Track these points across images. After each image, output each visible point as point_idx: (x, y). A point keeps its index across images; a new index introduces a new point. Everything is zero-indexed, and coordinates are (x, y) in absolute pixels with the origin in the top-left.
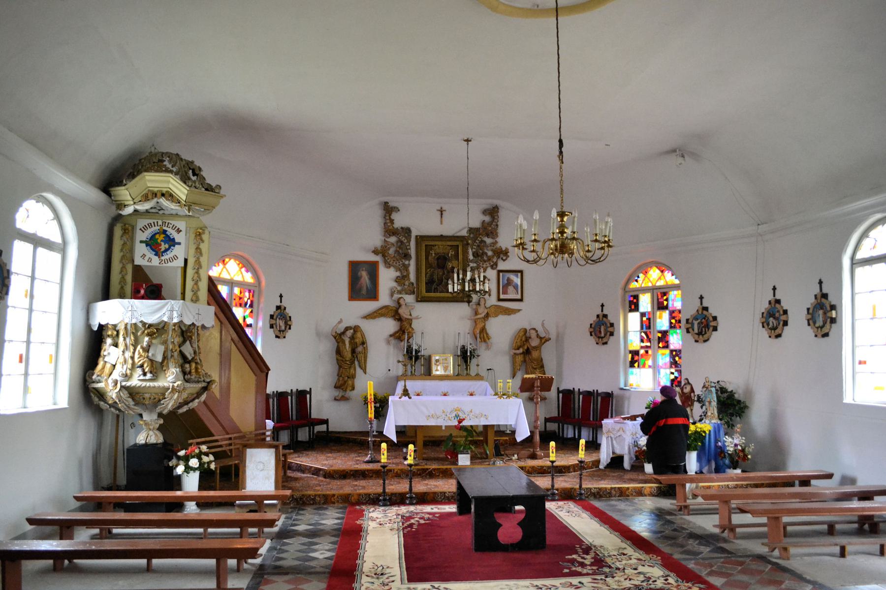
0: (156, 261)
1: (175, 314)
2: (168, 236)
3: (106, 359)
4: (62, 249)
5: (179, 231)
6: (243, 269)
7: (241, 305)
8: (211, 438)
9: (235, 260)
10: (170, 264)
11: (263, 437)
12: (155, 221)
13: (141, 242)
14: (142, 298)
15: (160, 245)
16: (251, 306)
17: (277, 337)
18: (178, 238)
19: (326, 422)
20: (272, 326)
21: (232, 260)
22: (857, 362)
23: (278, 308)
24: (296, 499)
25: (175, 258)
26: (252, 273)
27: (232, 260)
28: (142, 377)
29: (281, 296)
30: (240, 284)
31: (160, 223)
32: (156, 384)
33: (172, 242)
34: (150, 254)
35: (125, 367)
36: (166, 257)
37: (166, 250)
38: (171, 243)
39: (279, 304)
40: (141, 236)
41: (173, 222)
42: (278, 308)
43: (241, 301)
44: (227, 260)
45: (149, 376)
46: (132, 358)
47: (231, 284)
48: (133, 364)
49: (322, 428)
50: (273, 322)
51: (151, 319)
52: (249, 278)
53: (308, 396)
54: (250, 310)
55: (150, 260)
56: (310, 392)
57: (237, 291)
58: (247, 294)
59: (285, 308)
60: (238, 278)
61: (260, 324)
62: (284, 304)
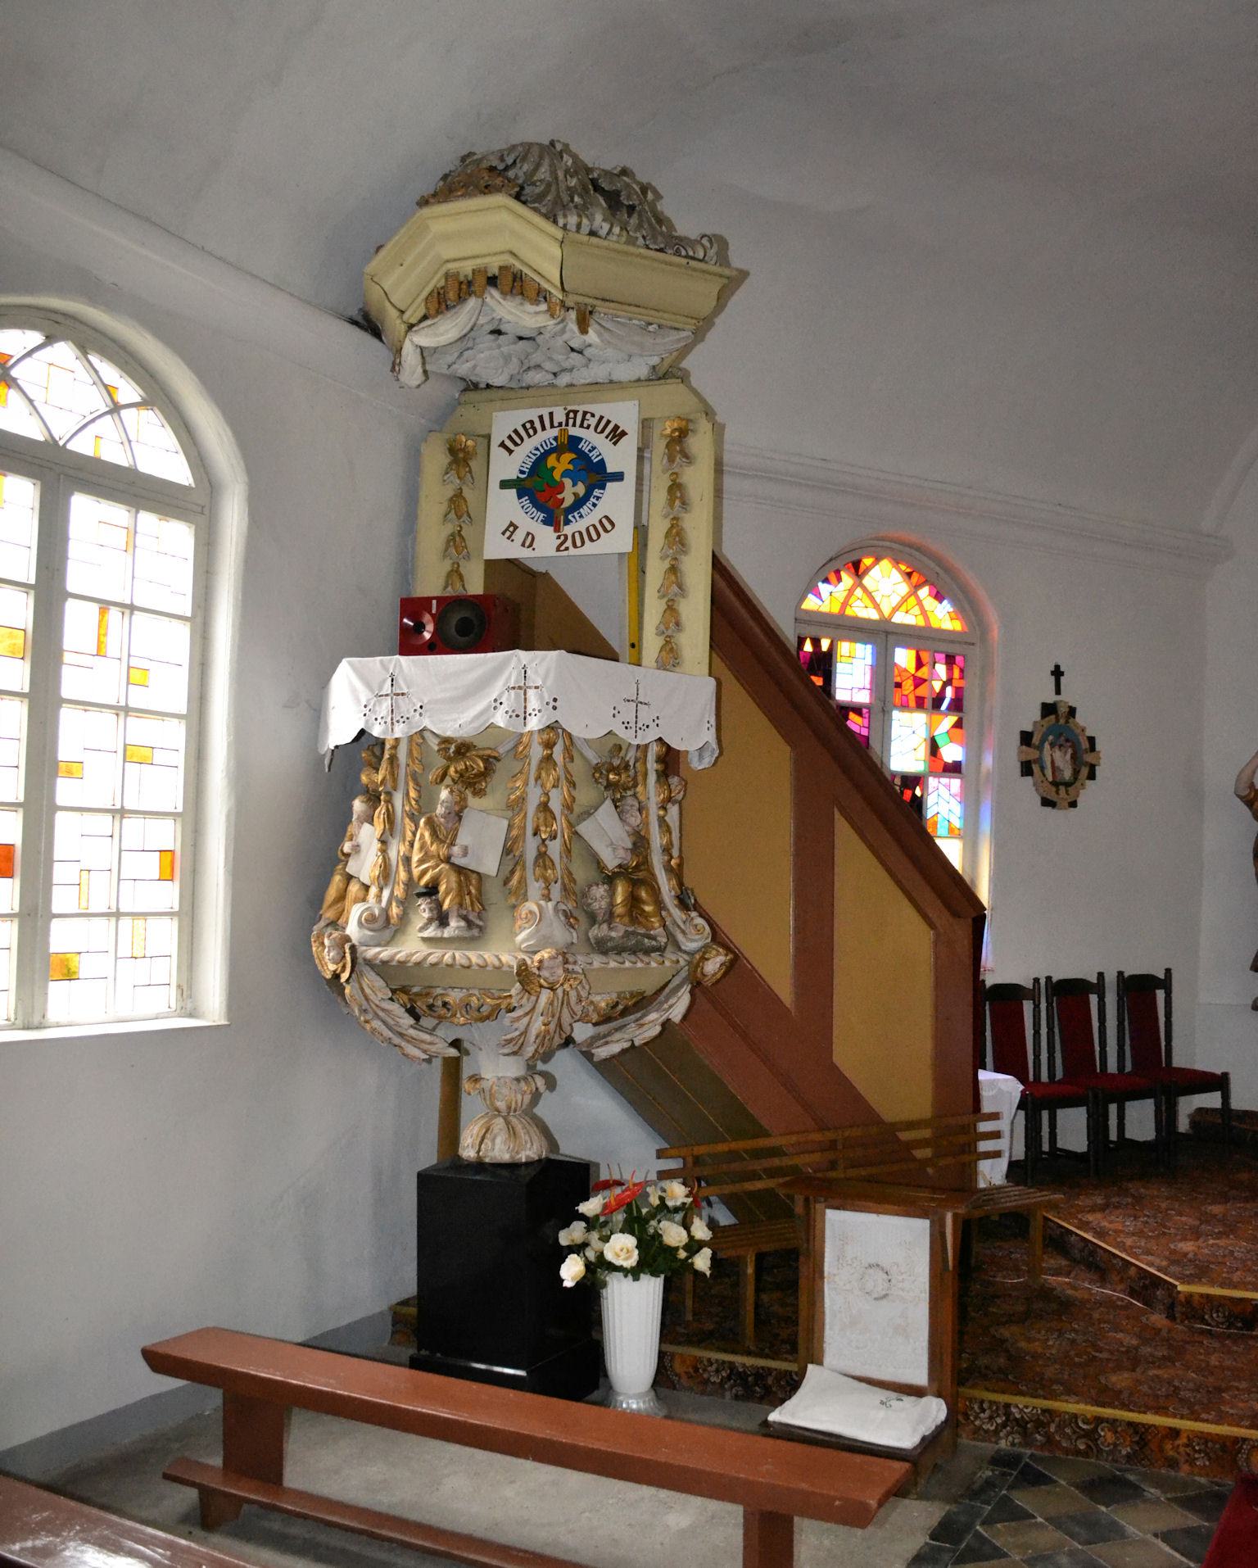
0: (546, 539)
1: (533, 703)
2: (583, 456)
3: (351, 868)
4: (188, 504)
5: (617, 435)
6: (924, 592)
7: (920, 703)
8: (763, 1143)
9: (896, 562)
10: (589, 548)
11: (962, 1139)
12: (545, 412)
13: (505, 485)
14: (431, 648)
15: (561, 488)
16: (957, 705)
17: (1047, 802)
18: (619, 457)
19: (1219, 1083)
20: (1027, 769)
21: (885, 564)
22: (111, 979)
23: (1048, 709)
24: (1021, 1424)
25: (607, 524)
26: (955, 602)
27: (885, 564)
28: (431, 932)
29: (1057, 673)
30: (921, 638)
31: (560, 416)
32: (474, 957)
33: (596, 475)
34: (529, 521)
35: (386, 894)
36: (577, 525)
37: (579, 503)
38: (595, 478)
39: (1051, 698)
40: (507, 465)
41: (598, 409)
42: (1048, 709)
43: (922, 691)
44: (867, 561)
45: (455, 925)
46: (407, 860)
47: (883, 635)
48: (410, 883)
49: (1212, 1100)
50: (1032, 754)
51: (457, 723)
52: (943, 616)
53: (1160, 994)
54: (952, 719)
55: (529, 541)
56: (1166, 983)
57: (904, 658)
58: (941, 669)
59: (1072, 712)
60: (907, 618)
61: (988, 761)
62: (1069, 697)
